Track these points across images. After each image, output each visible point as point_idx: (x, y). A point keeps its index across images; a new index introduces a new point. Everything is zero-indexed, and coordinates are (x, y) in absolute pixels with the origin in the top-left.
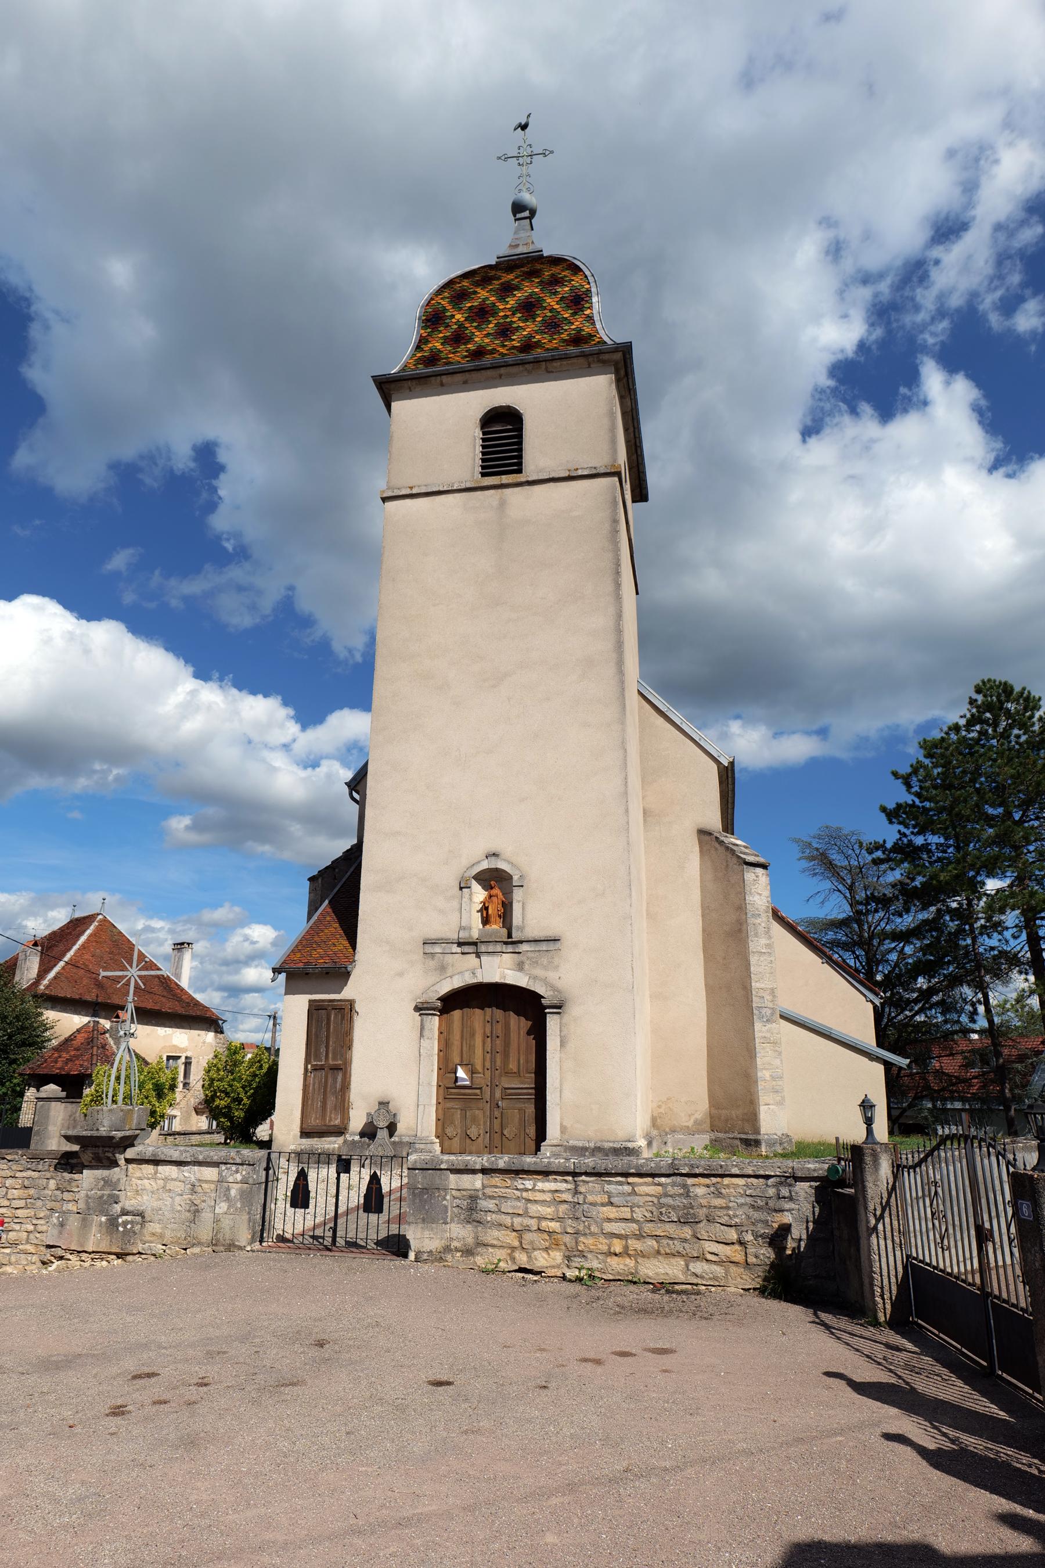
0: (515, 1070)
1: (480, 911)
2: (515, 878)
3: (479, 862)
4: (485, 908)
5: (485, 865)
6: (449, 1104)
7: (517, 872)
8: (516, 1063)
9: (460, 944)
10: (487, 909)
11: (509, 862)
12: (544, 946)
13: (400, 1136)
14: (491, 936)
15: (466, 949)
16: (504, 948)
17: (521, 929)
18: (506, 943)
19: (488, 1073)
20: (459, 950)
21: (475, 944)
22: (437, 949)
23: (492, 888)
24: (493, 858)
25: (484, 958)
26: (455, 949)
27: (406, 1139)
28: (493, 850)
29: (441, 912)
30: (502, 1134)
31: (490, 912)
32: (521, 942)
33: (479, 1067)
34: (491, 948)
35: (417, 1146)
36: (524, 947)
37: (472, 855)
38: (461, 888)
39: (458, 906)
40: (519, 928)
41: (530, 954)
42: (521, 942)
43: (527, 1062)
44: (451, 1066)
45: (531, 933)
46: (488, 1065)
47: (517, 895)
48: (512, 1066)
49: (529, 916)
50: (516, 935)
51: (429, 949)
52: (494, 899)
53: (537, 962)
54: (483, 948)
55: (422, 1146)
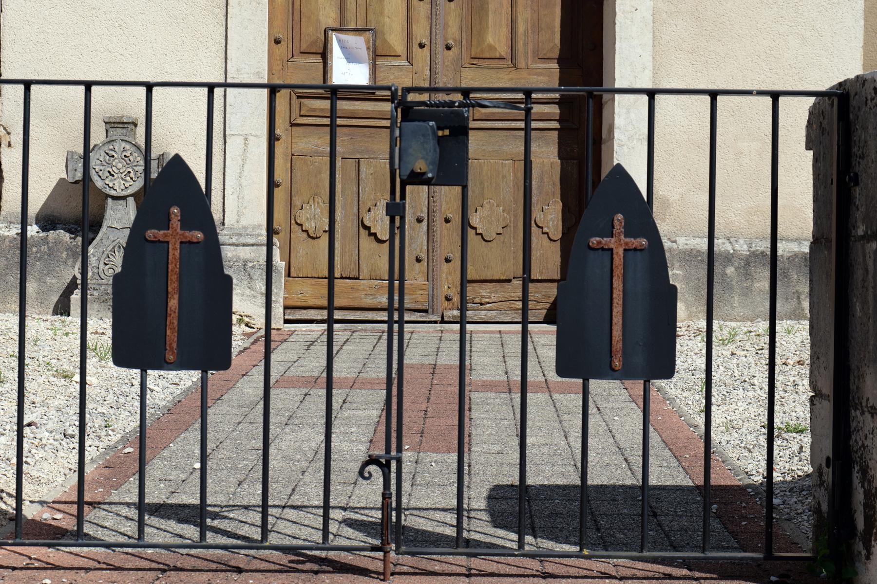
0: (503, 49)
8: (505, 30)
19: (422, 57)
30: (465, 224)
33: (396, 41)
43: (537, 27)
44: (310, 35)
46: (421, 33)
48: (496, 38)
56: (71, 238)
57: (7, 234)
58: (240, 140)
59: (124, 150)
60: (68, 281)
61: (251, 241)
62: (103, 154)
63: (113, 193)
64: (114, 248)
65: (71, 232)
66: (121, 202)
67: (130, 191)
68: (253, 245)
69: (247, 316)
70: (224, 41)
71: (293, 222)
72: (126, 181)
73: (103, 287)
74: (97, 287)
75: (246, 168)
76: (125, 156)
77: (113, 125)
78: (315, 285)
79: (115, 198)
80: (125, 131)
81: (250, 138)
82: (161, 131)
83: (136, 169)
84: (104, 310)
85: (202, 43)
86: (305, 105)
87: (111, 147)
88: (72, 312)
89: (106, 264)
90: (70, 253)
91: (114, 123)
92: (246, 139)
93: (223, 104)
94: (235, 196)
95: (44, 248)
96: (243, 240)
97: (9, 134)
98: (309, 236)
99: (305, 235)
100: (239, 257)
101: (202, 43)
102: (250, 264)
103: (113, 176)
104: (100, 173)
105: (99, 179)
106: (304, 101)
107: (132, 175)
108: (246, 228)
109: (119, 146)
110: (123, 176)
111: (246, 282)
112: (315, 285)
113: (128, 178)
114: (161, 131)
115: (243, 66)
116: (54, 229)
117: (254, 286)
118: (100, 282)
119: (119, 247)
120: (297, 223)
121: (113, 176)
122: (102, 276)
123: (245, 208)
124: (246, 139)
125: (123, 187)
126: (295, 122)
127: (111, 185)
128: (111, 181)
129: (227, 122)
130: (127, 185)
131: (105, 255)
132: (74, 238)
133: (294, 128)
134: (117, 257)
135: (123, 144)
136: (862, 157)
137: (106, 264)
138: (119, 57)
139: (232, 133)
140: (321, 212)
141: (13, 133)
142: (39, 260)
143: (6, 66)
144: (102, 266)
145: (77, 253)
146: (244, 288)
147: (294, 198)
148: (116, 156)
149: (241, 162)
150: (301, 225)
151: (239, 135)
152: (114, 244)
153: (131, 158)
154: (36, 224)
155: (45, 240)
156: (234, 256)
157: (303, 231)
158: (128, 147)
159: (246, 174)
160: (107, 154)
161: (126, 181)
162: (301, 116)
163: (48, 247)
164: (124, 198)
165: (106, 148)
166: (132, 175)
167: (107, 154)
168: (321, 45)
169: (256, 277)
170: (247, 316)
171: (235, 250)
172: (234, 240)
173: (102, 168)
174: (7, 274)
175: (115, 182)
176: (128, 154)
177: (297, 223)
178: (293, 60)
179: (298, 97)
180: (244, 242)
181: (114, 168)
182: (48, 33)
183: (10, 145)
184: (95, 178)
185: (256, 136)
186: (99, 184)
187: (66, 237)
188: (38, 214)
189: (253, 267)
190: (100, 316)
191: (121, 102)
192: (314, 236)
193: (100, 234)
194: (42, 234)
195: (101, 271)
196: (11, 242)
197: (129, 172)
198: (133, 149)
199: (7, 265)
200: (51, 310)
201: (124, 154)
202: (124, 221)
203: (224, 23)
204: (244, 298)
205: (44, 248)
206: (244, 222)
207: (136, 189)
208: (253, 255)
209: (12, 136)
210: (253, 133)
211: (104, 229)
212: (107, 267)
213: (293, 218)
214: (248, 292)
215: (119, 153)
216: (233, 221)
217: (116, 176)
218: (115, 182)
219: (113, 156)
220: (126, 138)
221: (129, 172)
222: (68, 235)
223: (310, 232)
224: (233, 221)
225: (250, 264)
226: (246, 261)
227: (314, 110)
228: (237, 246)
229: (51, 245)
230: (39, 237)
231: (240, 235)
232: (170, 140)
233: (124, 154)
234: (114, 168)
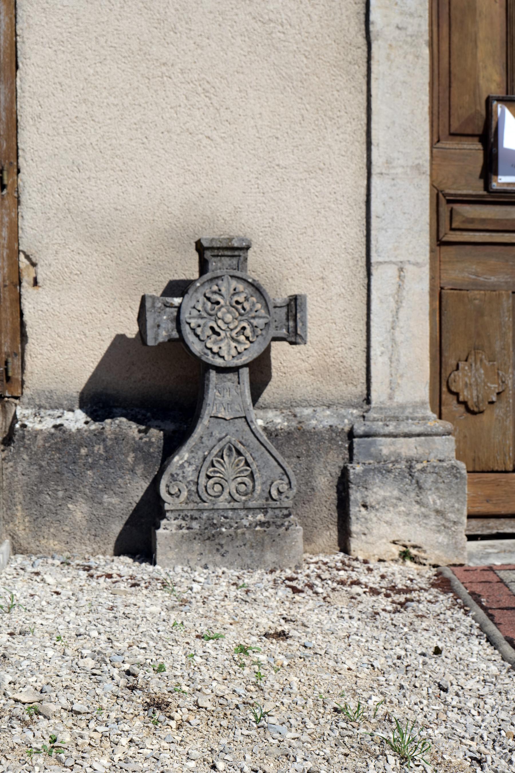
6: (463, 270)
13: (288, 406)
27: (323, 419)
35: (386, 447)
44: (466, 108)
55: (408, 448)
56: (140, 431)
57: (38, 427)
58: (392, 271)
59: (236, 292)
60: (137, 500)
61: (417, 429)
62: (202, 299)
63: (219, 362)
64: (222, 450)
65: (139, 422)
66: (230, 376)
67: (245, 359)
68: (419, 435)
69: (414, 547)
70: (364, 116)
71: (444, 389)
72: (238, 342)
73: (205, 515)
74: (196, 514)
75: (402, 314)
76: (237, 302)
77: (216, 252)
78: (478, 483)
79: (220, 370)
80: (235, 261)
81: (408, 268)
82: (272, 258)
83: (255, 322)
84: (210, 552)
85: (331, 119)
86: (458, 214)
87: (215, 288)
88: (159, 557)
89: (209, 477)
90: (140, 455)
91: (218, 248)
92: (401, 270)
93: (364, 214)
94: (386, 358)
95: (99, 449)
96: (404, 428)
97: (34, 265)
98: (468, 410)
99: (461, 409)
100: (399, 455)
101: (331, 119)
102: (419, 466)
103: (218, 334)
104: (199, 331)
105: (195, 340)
106: (457, 207)
107: (248, 332)
108: (402, 407)
109: (227, 286)
110: (234, 334)
111: (413, 495)
112: (478, 483)
113: (242, 338)
114: (272, 258)
115: (396, 155)
116: (112, 416)
117: (425, 500)
118: (201, 505)
119: (230, 449)
120: (450, 391)
121: (218, 334)
122: (204, 496)
123: (402, 376)
124: (401, 270)
125: (234, 352)
126: (445, 239)
127: (215, 350)
128: (215, 342)
129: (373, 242)
130: (241, 348)
131: (207, 463)
132: (145, 431)
133: (444, 248)
134: (227, 465)
135: (234, 283)
136: (237, 210)
137: (209, 477)
138: (205, 141)
139: (380, 259)
140: (486, 374)
141: (40, 263)
142: (91, 468)
143: (28, 156)
144: (203, 480)
145: (150, 454)
146: (410, 503)
147: (445, 354)
148: (222, 302)
149: (393, 305)
150: (457, 394)
151: (391, 262)
152: (222, 444)
153: (247, 305)
154: (81, 407)
155: (99, 435)
156: (391, 454)
157: (459, 402)
158: (241, 287)
159: (401, 324)
160: (209, 299)
161: (238, 342)
162: (452, 229)
163: (105, 447)
164: (235, 370)
165: (206, 290)
166: (248, 332)
167: (209, 299)
168: (481, 123)
169: (427, 486)
170: (414, 547)
171: (393, 444)
172: (391, 428)
173: (201, 322)
174: (41, 492)
175: (223, 345)
176: (241, 299)
177: (450, 391)
178: (439, 145)
179: (449, 202)
180: (406, 430)
181: (220, 322)
182: (93, 104)
183: (35, 283)
184: (190, 338)
185: (417, 264)
186: (196, 347)
187: (132, 429)
188: (82, 394)
189: (423, 470)
190: (203, 562)
191: (208, 213)
192: (476, 409)
193: (199, 430)
194: (94, 426)
195: (201, 489)
196: (46, 440)
197: (244, 328)
198: (249, 290)
199: (40, 477)
200: (111, 548)
201: (236, 298)
202: (237, 407)
203: (365, 88)
204: (411, 518)
205: (99, 449)
206: (399, 398)
207: (255, 355)
208: (421, 451)
209: (39, 269)
210: (412, 259)
211: (205, 422)
212: (211, 481)
213: (444, 383)
214: (416, 508)
215: (228, 298)
216: (384, 398)
217: (223, 334)
218: (223, 345)
219: (218, 303)
220: (238, 274)
221: (244, 328)
222: (134, 425)
223: (470, 404)
224: (384, 398)
225: (419, 466)
226: (410, 462)
227: (472, 221)
228: (395, 436)
229: (109, 443)
230: (91, 431)
231: (396, 419)
232: (285, 272)
233: (236, 298)
234: (220, 322)
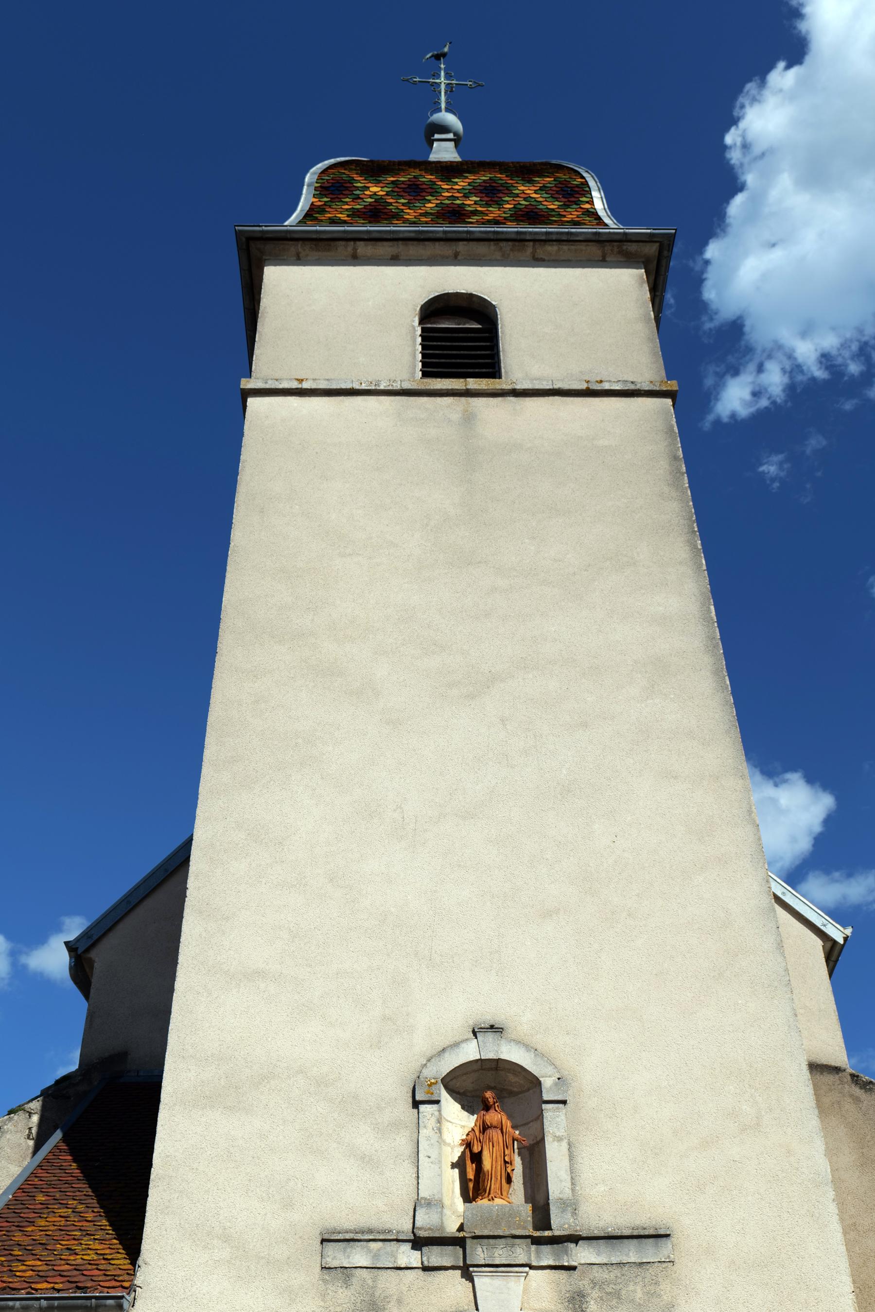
1: (459, 1165)
2: (547, 1083)
3: (456, 1045)
4: (471, 1159)
5: (470, 1052)
7: (550, 1070)
9: (418, 1243)
10: (477, 1158)
11: (527, 1047)
12: (631, 1253)
14: (497, 1223)
15: (436, 1256)
16: (521, 1253)
17: (572, 1205)
18: (537, 1241)
20: (413, 1258)
21: (458, 1242)
22: (359, 1257)
23: (487, 1108)
24: (490, 1037)
25: (483, 1281)
26: (408, 1256)
28: (489, 1018)
29: (367, 1161)
31: (487, 1164)
32: (575, 1239)
34: (500, 1255)
36: (582, 1254)
37: (440, 1028)
38: (416, 1104)
39: (409, 1149)
40: (565, 1204)
41: (598, 1274)
42: (575, 1239)
45: (597, 1215)
47: (554, 1122)
49: (586, 1175)
50: (560, 1223)
51: (337, 1256)
52: (496, 1134)
53: (617, 1295)
54: (479, 1254)
